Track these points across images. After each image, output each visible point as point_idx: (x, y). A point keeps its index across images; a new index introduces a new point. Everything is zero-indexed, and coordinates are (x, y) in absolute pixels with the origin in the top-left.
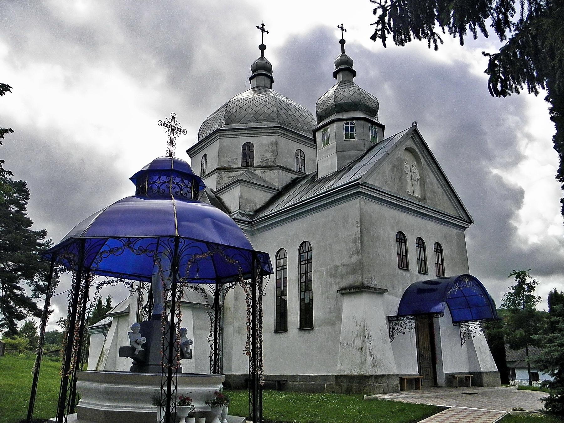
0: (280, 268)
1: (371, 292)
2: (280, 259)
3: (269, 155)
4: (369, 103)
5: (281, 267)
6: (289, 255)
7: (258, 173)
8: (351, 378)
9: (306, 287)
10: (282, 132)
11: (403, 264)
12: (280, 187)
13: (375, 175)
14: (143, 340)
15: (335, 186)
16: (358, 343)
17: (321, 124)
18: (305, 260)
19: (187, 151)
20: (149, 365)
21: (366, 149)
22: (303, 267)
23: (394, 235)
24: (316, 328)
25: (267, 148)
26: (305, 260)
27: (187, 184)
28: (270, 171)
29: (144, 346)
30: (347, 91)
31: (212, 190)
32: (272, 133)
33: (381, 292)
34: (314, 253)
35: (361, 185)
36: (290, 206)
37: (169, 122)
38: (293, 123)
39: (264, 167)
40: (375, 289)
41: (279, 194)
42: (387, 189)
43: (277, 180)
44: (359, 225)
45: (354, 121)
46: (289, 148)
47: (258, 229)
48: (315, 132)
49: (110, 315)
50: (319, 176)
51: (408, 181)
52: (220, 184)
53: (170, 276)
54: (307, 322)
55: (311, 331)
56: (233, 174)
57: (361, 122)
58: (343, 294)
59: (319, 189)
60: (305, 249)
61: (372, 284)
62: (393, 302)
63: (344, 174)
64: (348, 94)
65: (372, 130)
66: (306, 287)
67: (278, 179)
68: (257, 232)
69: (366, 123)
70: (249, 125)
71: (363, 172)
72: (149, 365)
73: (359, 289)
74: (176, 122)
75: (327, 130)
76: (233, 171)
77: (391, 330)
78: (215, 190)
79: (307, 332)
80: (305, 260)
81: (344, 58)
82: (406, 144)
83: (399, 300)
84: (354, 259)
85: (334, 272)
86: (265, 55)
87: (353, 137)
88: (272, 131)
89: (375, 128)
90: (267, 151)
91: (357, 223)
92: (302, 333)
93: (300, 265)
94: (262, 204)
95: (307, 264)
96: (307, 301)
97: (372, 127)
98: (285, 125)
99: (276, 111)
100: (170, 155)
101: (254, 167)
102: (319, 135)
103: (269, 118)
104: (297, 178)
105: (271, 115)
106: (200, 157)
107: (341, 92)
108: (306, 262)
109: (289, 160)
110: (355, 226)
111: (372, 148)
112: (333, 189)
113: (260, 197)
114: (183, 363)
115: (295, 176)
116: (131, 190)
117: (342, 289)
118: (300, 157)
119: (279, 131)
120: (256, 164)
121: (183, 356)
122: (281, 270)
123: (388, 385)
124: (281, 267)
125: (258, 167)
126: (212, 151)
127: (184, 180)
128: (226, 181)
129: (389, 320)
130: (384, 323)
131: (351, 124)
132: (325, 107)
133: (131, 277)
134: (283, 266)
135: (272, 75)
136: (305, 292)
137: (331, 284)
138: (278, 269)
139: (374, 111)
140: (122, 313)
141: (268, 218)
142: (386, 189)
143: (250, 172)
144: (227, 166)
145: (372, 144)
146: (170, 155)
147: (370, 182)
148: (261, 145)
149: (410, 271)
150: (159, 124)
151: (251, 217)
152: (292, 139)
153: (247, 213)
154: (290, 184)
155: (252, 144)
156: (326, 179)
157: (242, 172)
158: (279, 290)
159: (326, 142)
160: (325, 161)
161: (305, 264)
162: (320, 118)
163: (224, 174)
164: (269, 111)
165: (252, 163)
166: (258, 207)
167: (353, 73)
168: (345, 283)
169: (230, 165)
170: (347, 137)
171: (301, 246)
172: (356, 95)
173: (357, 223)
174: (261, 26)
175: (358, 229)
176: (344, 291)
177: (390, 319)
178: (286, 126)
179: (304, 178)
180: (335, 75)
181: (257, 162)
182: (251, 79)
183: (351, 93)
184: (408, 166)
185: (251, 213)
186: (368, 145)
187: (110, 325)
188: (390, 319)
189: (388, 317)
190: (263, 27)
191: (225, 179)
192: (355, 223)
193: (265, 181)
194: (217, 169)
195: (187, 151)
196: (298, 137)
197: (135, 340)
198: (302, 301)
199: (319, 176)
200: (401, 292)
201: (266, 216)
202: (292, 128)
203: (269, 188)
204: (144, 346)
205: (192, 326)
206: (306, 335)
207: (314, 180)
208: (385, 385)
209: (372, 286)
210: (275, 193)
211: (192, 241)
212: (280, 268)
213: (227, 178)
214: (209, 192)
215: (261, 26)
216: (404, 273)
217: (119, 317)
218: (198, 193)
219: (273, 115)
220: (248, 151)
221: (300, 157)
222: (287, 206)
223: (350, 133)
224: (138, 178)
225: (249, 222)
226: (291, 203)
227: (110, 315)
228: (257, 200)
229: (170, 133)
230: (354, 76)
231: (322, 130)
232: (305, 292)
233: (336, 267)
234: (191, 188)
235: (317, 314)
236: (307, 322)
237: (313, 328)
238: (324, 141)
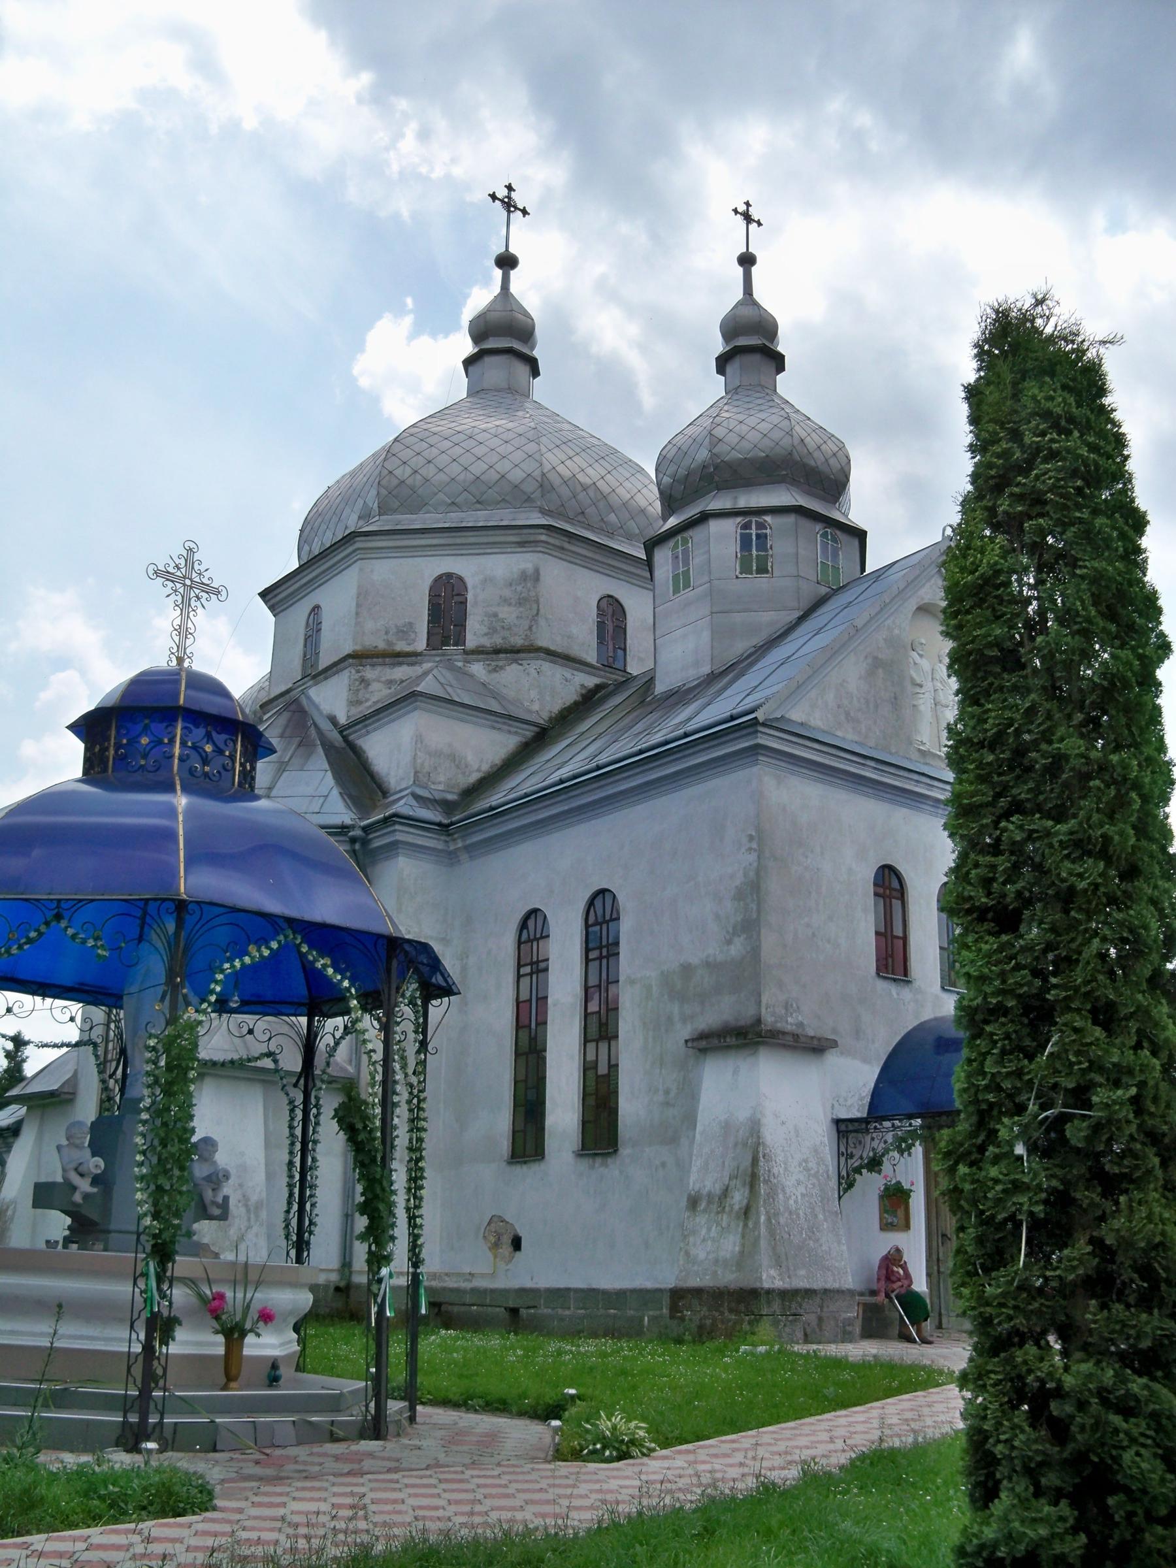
0: (527, 969)
1: (785, 1046)
2: (596, 923)
3: (508, 614)
4: (818, 460)
5: (531, 964)
6: (554, 928)
7: (478, 669)
8: (716, 1297)
9: (600, 1027)
10: (557, 542)
11: (893, 960)
12: (545, 715)
13: (813, 694)
14: (96, 1164)
15: (691, 727)
16: (738, 1198)
17: (672, 521)
18: (601, 945)
19: (264, 595)
20: (109, 1232)
21: (805, 604)
22: (525, 982)
23: (867, 873)
24: (625, 1151)
25: (507, 593)
26: (600, 948)
27: (222, 746)
28: (514, 666)
29: (96, 1180)
30: (752, 421)
31: (333, 720)
32: (521, 544)
33: (815, 1047)
34: (626, 926)
35: (764, 725)
36: (562, 782)
37: (177, 567)
38: (591, 511)
39: (504, 653)
40: (796, 1037)
41: (541, 737)
42: (850, 736)
43: (534, 694)
44: (754, 845)
45: (768, 518)
46: (571, 597)
47: (467, 848)
48: (652, 545)
49: (18, 1099)
50: (660, 688)
51: (922, 708)
52: (359, 703)
53: (162, 999)
54: (601, 1131)
55: (610, 1160)
56: (401, 672)
57: (790, 519)
58: (703, 1051)
59: (648, 730)
60: (601, 913)
61: (790, 1024)
62: (853, 1079)
63: (725, 688)
64: (749, 430)
65: (825, 546)
66: (600, 1027)
67: (543, 690)
68: (464, 857)
69: (805, 523)
70: (453, 519)
71: (774, 686)
72: (109, 1232)
73: (744, 1037)
74: (196, 567)
75: (685, 542)
76: (401, 664)
77: (843, 1160)
78: (342, 720)
79: (599, 1160)
80: (601, 945)
81: (747, 312)
82: (922, 592)
83: (877, 1071)
84: (737, 948)
85: (680, 984)
86: (514, 289)
87: (762, 570)
88: (523, 538)
89: (835, 540)
90: (505, 601)
91: (751, 838)
92: (584, 1164)
93: (587, 960)
94: (485, 767)
95: (608, 957)
96: (603, 1069)
97: (825, 535)
98: (561, 519)
99: (537, 474)
100: (180, 660)
101: (465, 652)
102: (663, 557)
103: (516, 495)
104: (598, 688)
105: (524, 487)
106: (299, 614)
107: (732, 424)
108: (604, 953)
109: (574, 630)
110: (743, 850)
111: (821, 602)
112: (686, 735)
113: (483, 747)
114: (205, 1230)
115: (591, 681)
116: (66, 761)
117: (703, 1036)
118: (612, 615)
119: (543, 538)
120: (471, 641)
121: (204, 1213)
122: (531, 974)
123: (820, 1319)
124: (531, 964)
125: (479, 652)
126: (337, 598)
127: (214, 734)
128: (379, 694)
129: (839, 1132)
130: (821, 1136)
131: (761, 526)
132: (682, 472)
133: (70, 994)
134: (538, 962)
135: (536, 353)
136: (597, 1041)
137: (670, 1019)
138: (523, 971)
139: (831, 482)
140: (52, 1094)
141: (496, 814)
142: (847, 736)
143: (452, 668)
144: (382, 645)
145: (824, 590)
146: (180, 660)
147: (796, 715)
148: (487, 581)
149: (916, 984)
150: (151, 572)
151: (447, 806)
152: (589, 564)
153: (438, 796)
154: (576, 703)
155: (460, 579)
156: (679, 697)
157: (427, 666)
158: (524, 1034)
159: (682, 581)
160: (672, 640)
161: (600, 958)
162: (670, 502)
163: (369, 673)
164: (517, 476)
165: (460, 640)
166: (474, 777)
167: (778, 362)
168: (712, 1017)
169: (389, 643)
170: (746, 568)
171: (591, 903)
172: (776, 435)
173: (751, 838)
174: (502, 193)
175: (753, 857)
176: (703, 1044)
177: (844, 1129)
178: (569, 520)
179: (620, 686)
180: (722, 363)
181: (475, 633)
182: (469, 363)
183: (765, 427)
184: (925, 664)
185: (450, 797)
186: (810, 591)
187: (15, 1130)
188: (844, 1129)
189: (838, 1122)
190: (509, 197)
191: (375, 686)
192: (745, 840)
193: (495, 695)
194: (349, 656)
195: (264, 595)
196: (602, 556)
197: (74, 1165)
198: (588, 1068)
199: (660, 688)
200: (883, 1042)
201: (492, 808)
202: (589, 527)
203: (510, 717)
204: (96, 1180)
205: (236, 1131)
206: (611, 1170)
207: (646, 697)
208: (812, 1318)
209: (789, 1028)
210: (529, 733)
211: (222, 910)
212: (527, 969)
213: (381, 684)
214: (326, 726)
215: (502, 193)
216: (893, 989)
217: (44, 1106)
218: (253, 768)
219: (529, 487)
220: (447, 606)
221: (612, 615)
222: (555, 777)
223: (754, 555)
224: (91, 727)
225: (439, 824)
226: (565, 772)
227: (18, 1099)
228: (470, 758)
229: (179, 598)
230: (781, 368)
231: (671, 543)
232: (597, 1041)
233: (687, 970)
234: (232, 757)
235: (632, 1107)
236: (601, 1131)
237: (616, 1151)
238: (676, 578)
